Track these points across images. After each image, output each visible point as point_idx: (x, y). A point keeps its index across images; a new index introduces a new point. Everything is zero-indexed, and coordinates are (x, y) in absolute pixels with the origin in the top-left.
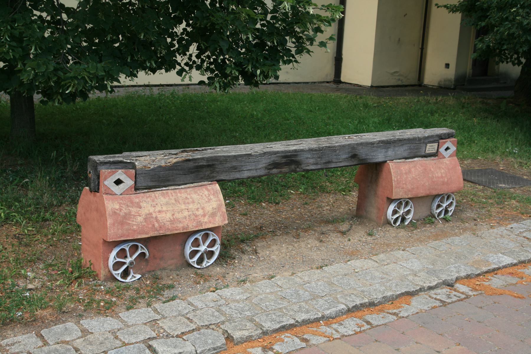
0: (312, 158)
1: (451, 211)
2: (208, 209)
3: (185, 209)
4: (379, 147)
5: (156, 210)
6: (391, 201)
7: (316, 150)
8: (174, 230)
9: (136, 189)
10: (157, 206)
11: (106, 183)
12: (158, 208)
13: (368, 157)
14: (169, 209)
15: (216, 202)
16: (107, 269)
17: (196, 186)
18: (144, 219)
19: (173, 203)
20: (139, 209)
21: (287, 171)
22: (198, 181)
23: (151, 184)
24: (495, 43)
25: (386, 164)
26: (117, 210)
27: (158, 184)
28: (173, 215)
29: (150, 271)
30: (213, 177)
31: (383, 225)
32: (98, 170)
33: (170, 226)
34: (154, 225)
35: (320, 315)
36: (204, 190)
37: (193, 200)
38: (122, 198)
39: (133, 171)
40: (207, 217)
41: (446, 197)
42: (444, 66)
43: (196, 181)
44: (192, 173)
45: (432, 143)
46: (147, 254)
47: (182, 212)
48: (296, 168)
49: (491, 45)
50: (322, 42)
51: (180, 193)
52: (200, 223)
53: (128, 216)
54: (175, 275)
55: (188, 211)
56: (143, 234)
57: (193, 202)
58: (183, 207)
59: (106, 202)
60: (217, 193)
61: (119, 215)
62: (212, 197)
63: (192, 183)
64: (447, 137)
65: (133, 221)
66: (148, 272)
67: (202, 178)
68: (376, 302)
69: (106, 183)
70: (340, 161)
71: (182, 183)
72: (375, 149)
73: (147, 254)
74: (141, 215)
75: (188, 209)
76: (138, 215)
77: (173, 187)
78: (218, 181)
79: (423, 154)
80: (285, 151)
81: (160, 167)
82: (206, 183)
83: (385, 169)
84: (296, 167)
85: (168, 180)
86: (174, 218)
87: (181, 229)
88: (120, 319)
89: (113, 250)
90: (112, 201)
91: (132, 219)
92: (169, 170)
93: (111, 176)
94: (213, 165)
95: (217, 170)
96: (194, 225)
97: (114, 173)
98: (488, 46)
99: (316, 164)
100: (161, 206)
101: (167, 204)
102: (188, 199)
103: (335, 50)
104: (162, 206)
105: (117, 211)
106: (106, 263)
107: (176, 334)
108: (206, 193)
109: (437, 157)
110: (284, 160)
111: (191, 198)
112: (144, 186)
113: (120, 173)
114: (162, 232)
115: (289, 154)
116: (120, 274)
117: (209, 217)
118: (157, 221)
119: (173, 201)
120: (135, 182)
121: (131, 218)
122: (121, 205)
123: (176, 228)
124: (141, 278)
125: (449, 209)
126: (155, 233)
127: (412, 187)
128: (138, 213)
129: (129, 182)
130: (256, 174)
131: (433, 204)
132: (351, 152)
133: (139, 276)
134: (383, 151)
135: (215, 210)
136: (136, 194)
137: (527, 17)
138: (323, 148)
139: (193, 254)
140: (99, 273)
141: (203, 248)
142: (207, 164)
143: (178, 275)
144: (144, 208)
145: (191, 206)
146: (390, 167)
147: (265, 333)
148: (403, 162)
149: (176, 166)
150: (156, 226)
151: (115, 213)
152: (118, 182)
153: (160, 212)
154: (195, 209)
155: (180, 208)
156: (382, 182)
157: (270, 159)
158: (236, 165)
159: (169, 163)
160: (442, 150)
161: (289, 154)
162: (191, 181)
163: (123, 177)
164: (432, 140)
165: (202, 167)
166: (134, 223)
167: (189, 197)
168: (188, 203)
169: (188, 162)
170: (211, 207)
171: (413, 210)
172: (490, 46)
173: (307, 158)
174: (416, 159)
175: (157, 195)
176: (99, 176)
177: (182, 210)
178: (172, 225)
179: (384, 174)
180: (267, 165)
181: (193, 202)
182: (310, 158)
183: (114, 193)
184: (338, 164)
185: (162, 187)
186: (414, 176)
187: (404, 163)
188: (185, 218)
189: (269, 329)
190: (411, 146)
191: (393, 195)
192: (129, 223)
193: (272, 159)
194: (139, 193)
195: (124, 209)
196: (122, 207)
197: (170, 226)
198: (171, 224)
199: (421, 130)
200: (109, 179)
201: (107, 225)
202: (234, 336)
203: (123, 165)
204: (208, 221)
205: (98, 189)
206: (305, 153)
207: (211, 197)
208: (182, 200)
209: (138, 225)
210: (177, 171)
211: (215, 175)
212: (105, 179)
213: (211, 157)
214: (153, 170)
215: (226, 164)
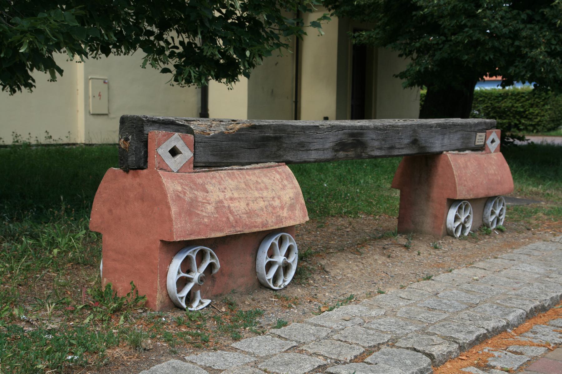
0: (377, 140)
1: (502, 219)
2: (284, 199)
3: (260, 197)
4: (437, 132)
5: (227, 196)
6: (452, 202)
7: (380, 129)
8: (252, 227)
9: (195, 167)
10: (226, 191)
11: (160, 151)
12: (228, 195)
13: (427, 145)
14: (241, 196)
15: (292, 190)
16: (164, 292)
17: (263, 168)
18: (215, 208)
19: (243, 188)
20: (206, 194)
21: (353, 156)
22: (264, 160)
23: (212, 159)
24: (433, 65)
25: (442, 156)
26: (180, 192)
27: (219, 160)
28: (248, 204)
29: (217, 296)
30: (280, 156)
31: (444, 236)
32: (146, 132)
33: (247, 220)
34: (228, 218)
35: (504, 323)
36: (274, 172)
37: (266, 186)
38: (182, 176)
39: (192, 137)
40: (285, 210)
41: (498, 201)
42: (326, 116)
43: (262, 161)
44: (258, 147)
45: (481, 132)
46: (218, 265)
47: (257, 200)
48: (361, 153)
49: (430, 66)
50: (314, 22)
51: (249, 175)
52: (280, 219)
53: (194, 203)
54: (250, 300)
55: (264, 201)
56: (216, 231)
57: (267, 188)
58: (256, 194)
59: (164, 180)
60: (289, 176)
61: (185, 200)
62: (285, 182)
63: (257, 163)
64: (490, 127)
65: (202, 211)
66: (215, 296)
67: (268, 157)
68: (546, 305)
69: (160, 151)
70: (402, 146)
71: (246, 161)
72: (433, 134)
73: (218, 265)
74: (210, 202)
75: (262, 198)
76: (207, 203)
77: (237, 167)
78: (288, 163)
79: (473, 146)
80: (352, 126)
81: (222, 133)
82: (273, 164)
83: (441, 163)
84: (362, 151)
85: (232, 156)
86: (249, 209)
87: (261, 226)
88: (239, 351)
89: (172, 259)
90: (171, 179)
91: (200, 208)
92: (233, 140)
93: (165, 140)
94: (281, 137)
95: (285, 145)
96: (273, 220)
97: (169, 137)
98: (426, 68)
99: (380, 149)
100: (231, 191)
101: (237, 189)
102: (260, 183)
103: (200, 105)
104: (233, 192)
105: (181, 195)
106: (163, 281)
107: (349, 358)
108: (278, 176)
109: (484, 152)
110: (350, 140)
111: (263, 182)
112: (204, 163)
113: (177, 138)
114: (239, 230)
115: (356, 131)
116: (184, 298)
117: (288, 210)
118: (231, 212)
119: (244, 186)
120: (194, 154)
121: (199, 206)
122: (184, 186)
123: (255, 224)
124: (211, 302)
125: (501, 218)
126: (231, 230)
127: (473, 185)
128: (205, 199)
129: (187, 154)
130: (323, 157)
131: (486, 210)
132: (413, 136)
133: (207, 302)
134: (440, 137)
135: (293, 201)
136: (195, 172)
137: (493, 20)
138: (387, 126)
139: (270, 265)
140: (150, 300)
141: (280, 258)
142: (274, 135)
143: (253, 300)
144: (212, 192)
145: (265, 194)
146: (448, 159)
147: (461, 348)
148: (458, 154)
149: (240, 134)
150: (231, 220)
151: (178, 198)
152: (174, 152)
153: (231, 199)
154: (270, 198)
155: (253, 196)
156: (439, 179)
157: (337, 135)
158: (304, 140)
159: (231, 129)
160: (488, 142)
161: (356, 131)
162: (256, 160)
163: (180, 145)
164: (481, 128)
165: (268, 139)
166: (204, 214)
167: (259, 181)
168: (261, 189)
169: (254, 130)
170: (288, 196)
171: (472, 216)
172: (429, 67)
173: (372, 139)
174: (467, 152)
175: (222, 176)
176: (147, 142)
177: (256, 199)
178: (250, 219)
179: (440, 169)
180: (334, 144)
181: (267, 188)
182: (375, 140)
183: (169, 169)
184: (400, 150)
185: (224, 166)
186: (471, 171)
187: (458, 156)
188: (262, 209)
189: (465, 341)
190: (463, 134)
191: (457, 194)
192: (198, 214)
193: (339, 137)
194: (198, 172)
195: (188, 192)
196: (185, 189)
197: (247, 220)
198: (247, 217)
199: (460, 119)
200: (163, 146)
201: (170, 216)
202: (434, 353)
203: (176, 127)
204: (288, 216)
205: (146, 162)
206: (370, 132)
207: (285, 182)
208: (253, 184)
209: (209, 217)
210: (241, 143)
211: (281, 153)
212: (159, 145)
213: (278, 125)
214: (213, 137)
215: (293, 137)
